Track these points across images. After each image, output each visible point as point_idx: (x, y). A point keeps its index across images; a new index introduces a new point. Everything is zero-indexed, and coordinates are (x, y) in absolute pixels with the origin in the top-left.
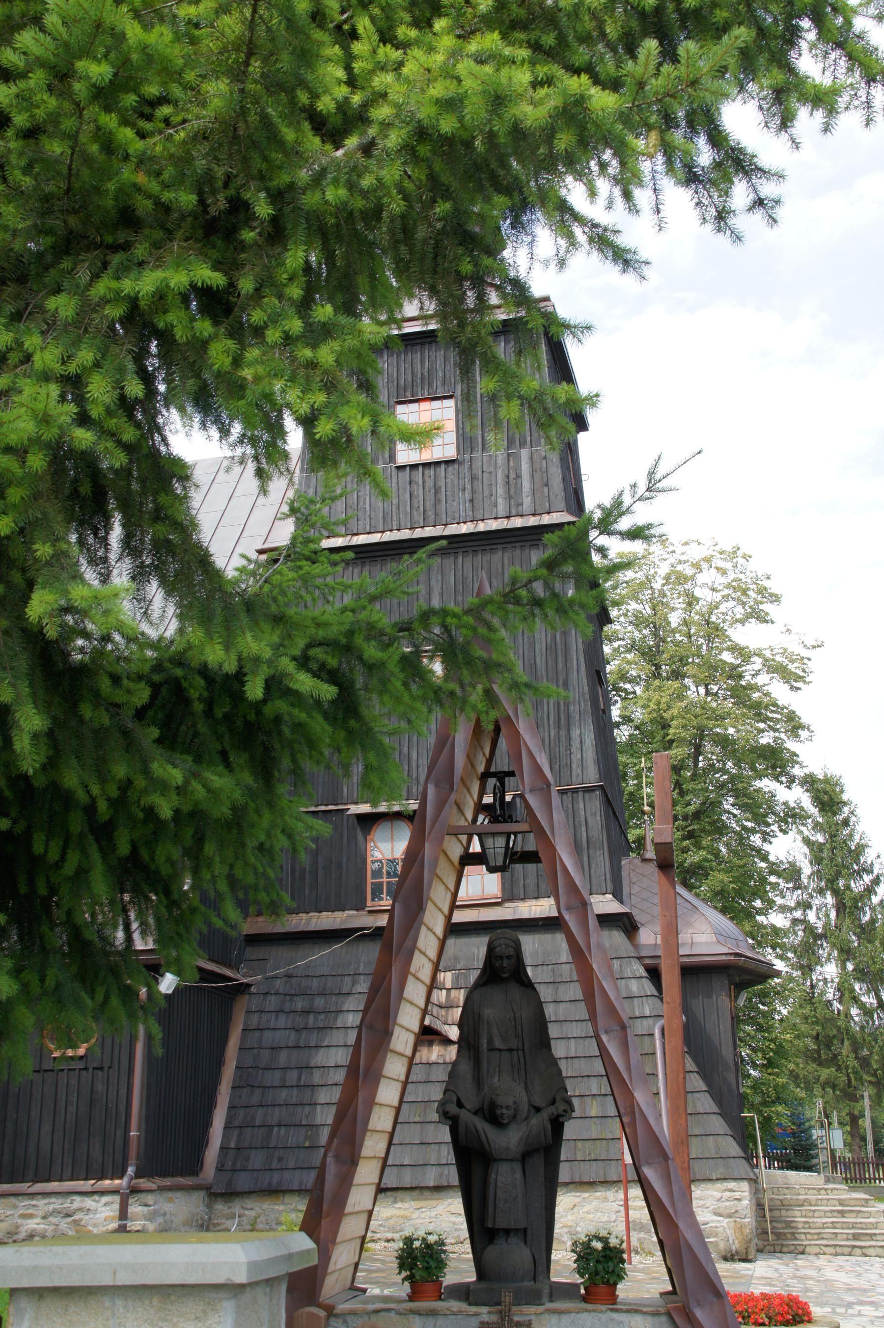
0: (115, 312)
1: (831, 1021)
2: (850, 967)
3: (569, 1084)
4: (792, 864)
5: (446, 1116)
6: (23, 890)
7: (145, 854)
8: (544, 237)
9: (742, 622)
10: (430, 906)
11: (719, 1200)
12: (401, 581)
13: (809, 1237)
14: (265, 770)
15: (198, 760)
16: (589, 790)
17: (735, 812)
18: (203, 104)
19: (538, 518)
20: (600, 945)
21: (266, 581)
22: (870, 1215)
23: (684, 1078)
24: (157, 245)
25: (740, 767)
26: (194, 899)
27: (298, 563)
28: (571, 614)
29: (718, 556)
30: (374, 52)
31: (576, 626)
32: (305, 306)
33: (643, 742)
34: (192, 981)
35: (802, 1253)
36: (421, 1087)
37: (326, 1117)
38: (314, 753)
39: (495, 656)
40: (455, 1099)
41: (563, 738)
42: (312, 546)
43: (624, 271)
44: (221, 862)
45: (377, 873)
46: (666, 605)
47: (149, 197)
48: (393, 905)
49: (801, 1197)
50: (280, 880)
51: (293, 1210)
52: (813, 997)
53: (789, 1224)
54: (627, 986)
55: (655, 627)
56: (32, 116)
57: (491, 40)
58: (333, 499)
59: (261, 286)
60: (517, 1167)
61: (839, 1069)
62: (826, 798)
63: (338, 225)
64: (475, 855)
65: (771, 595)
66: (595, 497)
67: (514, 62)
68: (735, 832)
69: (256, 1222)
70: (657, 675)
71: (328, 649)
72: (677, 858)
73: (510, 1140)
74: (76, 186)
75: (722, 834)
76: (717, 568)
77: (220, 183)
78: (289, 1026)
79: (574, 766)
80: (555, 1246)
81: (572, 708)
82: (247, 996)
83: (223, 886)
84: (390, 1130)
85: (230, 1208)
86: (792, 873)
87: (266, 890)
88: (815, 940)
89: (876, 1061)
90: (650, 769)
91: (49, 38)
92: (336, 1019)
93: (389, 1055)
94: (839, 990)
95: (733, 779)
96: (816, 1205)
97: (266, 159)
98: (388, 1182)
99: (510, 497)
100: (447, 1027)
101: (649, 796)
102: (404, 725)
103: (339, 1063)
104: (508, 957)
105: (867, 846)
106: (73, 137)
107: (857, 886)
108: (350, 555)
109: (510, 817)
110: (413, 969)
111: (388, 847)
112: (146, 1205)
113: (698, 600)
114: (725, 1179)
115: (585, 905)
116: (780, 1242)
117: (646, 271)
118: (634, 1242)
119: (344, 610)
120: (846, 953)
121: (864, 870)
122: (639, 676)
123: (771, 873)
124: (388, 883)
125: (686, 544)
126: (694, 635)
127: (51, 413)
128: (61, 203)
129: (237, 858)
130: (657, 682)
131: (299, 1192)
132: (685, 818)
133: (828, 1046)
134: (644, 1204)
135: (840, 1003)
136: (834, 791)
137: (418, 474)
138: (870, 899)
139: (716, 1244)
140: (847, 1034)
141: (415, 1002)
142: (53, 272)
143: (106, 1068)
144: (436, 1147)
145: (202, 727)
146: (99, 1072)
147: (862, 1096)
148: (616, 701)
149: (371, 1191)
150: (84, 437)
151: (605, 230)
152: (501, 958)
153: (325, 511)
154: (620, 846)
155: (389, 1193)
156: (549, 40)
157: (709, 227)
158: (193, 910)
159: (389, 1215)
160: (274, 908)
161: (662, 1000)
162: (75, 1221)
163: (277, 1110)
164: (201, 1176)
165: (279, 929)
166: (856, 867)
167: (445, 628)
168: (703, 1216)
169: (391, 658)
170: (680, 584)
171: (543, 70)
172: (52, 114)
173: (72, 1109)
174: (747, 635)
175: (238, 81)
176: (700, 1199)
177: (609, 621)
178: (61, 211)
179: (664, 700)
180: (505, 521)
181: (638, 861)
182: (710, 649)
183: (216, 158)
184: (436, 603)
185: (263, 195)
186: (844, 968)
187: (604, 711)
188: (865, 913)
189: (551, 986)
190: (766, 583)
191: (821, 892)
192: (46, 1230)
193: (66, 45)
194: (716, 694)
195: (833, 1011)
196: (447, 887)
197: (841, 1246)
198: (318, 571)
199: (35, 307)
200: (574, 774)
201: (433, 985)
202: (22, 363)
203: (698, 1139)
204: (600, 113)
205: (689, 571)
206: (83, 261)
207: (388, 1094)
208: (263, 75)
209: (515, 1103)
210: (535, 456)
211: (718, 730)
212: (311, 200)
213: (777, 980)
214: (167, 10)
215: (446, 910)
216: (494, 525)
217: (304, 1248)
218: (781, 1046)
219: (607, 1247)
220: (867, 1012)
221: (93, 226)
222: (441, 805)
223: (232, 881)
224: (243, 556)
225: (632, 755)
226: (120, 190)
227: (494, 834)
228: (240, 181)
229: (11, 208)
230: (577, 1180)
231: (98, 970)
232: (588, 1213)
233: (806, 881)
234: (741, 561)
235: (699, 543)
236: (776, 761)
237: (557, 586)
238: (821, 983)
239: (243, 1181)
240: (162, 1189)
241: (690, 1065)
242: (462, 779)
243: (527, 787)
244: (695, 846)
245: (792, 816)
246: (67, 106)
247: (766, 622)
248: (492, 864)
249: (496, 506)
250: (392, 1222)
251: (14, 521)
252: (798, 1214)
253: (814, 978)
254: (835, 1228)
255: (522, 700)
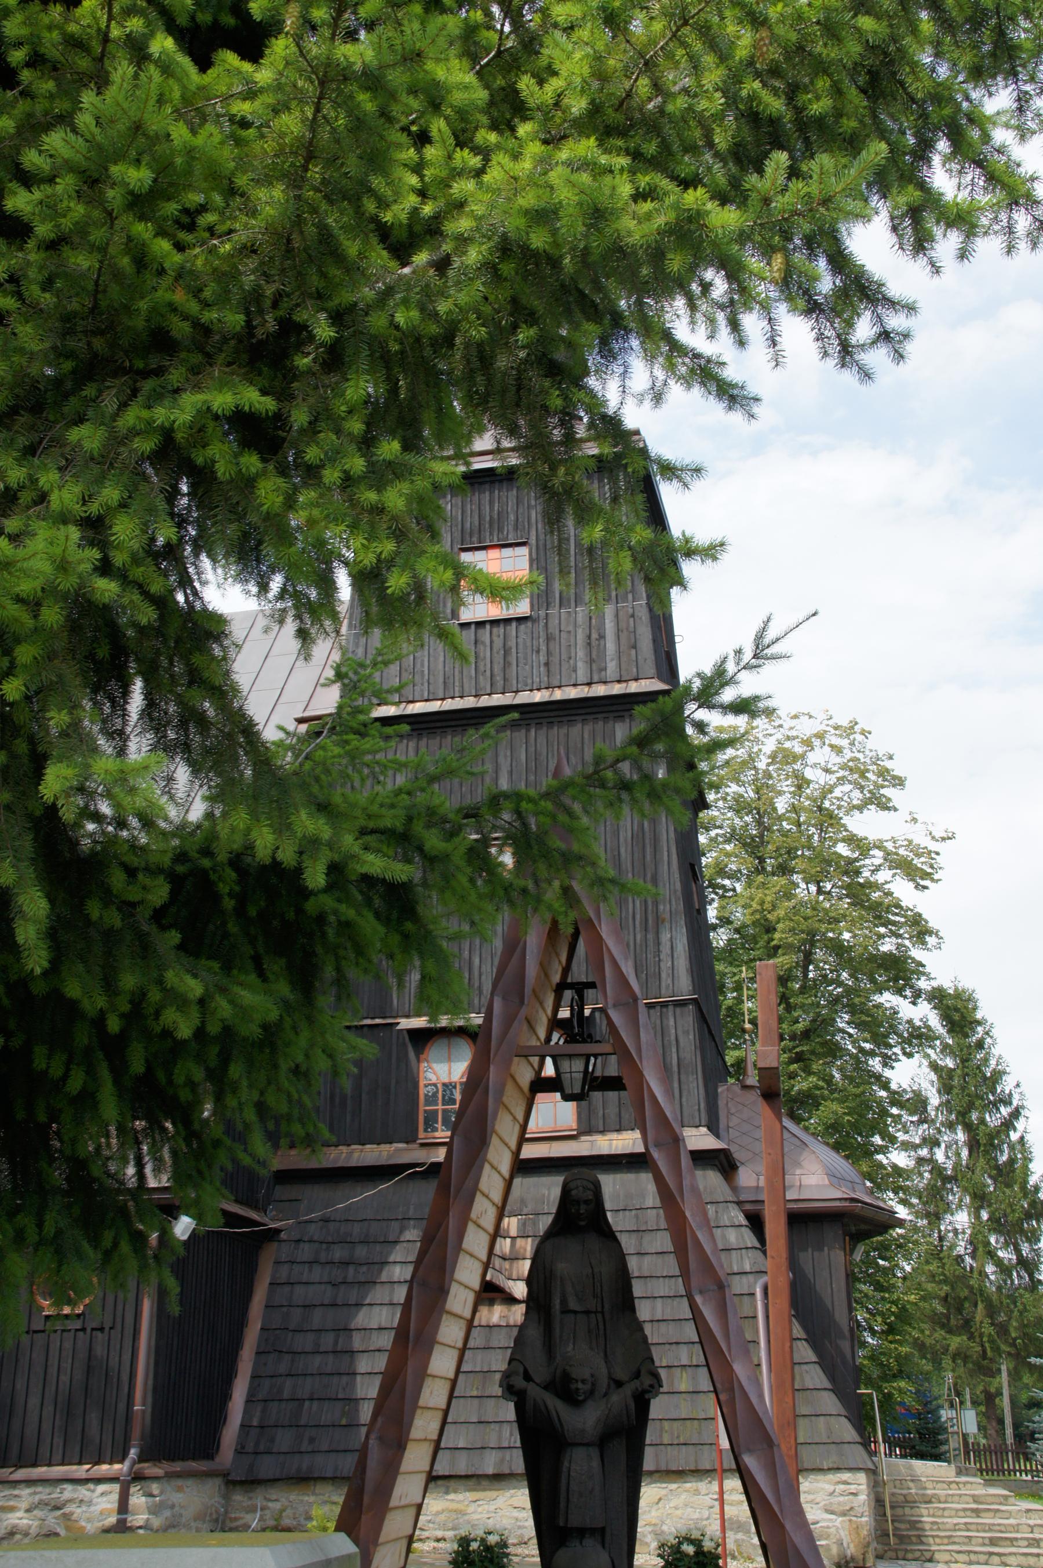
0: (146, 445)
1: (963, 1278)
2: (985, 1215)
3: (655, 1352)
4: (917, 1094)
5: (510, 1390)
6: (20, 1115)
7: (161, 1076)
8: (641, 371)
9: (860, 808)
10: (495, 1141)
11: (832, 1494)
12: (465, 760)
13: (938, 1540)
14: (305, 979)
15: (227, 967)
16: (681, 1004)
17: (851, 1031)
18: (253, 213)
19: (624, 685)
20: (695, 1189)
21: (307, 758)
22: (1009, 1515)
23: (791, 1347)
24: (195, 370)
25: (857, 979)
26: (217, 1131)
27: (345, 737)
28: (665, 799)
29: (833, 731)
30: (450, 157)
31: (669, 812)
32: (367, 443)
33: (744, 948)
34: (215, 1224)
35: (930, 1560)
36: (480, 1355)
37: (369, 1389)
38: (361, 960)
39: (576, 847)
40: (521, 1370)
41: (651, 943)
42: (361, 717)
43: (730, 408)
44: (250, 1086)
45: (431, 1099)
46: (771, 788)
47: (186, 318)
48: (452, 1138)
49: (929, 1492)
50: (317, 1110)
51: (324, 1505)
52: (941, 1251)
53: (914, 1525)
54: (724, 1237)
55: (758, 813)
56: (57, 226)
57: (586, 147)
58: (386, 663)
59: (316, 419)
60: (594, 1452)
61: (971, 1337)
62: (956, 1017)
63: (402, 352)
64: (549, 1079)
65: (894, 777)
66: (692, 662)
67: (611, 172)
68: (851, 1055)
69: (281, 1517)
70: (760, 870)
71: (383, 838)
72: (784, 1086)
73: (587, 1420)
74: (103, 304)
75: (835, 1057)
76: (831, 746)
77: (268, 303)
78: (325, 1279)
79: (664, 975)
80: (637, 1548)
81: (661, 907)
82: (275, 1244)
83: (250, 1115)
84: (444, 1407)
85: (250, 1498)
86: (917, 1104)
87: (301, 1120)
88: (944, 1184)
89: (1016, 1328)
90: (752, 980)
91: (81, 140)
92: (380, 1271)
93: (444, 1316)
94: (971, 1243)
95: (848, 991)
96: (946, 1502)
97: (323, 275)
98: (440, 1469)
99: (592, 661)
100: (511, 1283)
101: (750, 1011)
102: (466, 928)
103: (383, 1325)
104: (586, 1202)
105: (1005, 1073)
106: (102, 249)
107: (993, 1120)
108: (405, 728)
109: (590, 1036)
110: (473, 1215)
111: (445, 1070)
112: (151, 1495)
113: (808, 782)
114: (838, 1469)
115: (677, 1141)
116: (903, 1547)
117: (756, 409)
118: (731, 1545)
119: (398, 792)
120: (980, 1199)
121: (1001, 1101)
122: (740, 871)
123: (894, 1103)
124: (444, 1111)
125: (796, 717)
126: (804, 823)
127: (70, 559)
128: (85, 323)
129: (269, 1083)
130: (760, 878)
131: (334, 1479)
132: (793, 1038)
133: (959, 1310)
134: (743, 1498)
135: (973, 1258)
136: (966, 1008)
137: (485, 634)
138: (1008, 1136)
139: (827, 1548)
140: (981, 1295)
141: (476, 1253)
142: (73, 400)
143: (107, 1330)
144: (496, 1427)
145: (233, 927)
146: (99, 1334)
147: (999, 1371)
148: (713, 900)
149: (421, 1480)
150: (106, 588)
151: (709, 361)
152: (578, 1202)
153: (377, 675)
154: (716, 1070)
155: (440, 1482)
156: (651, 148)
157: (832, 362)
158: (217, 1144)
159: (440, 1508)
160: (310, 1141)
161: (764, 1253)
162: (64, 1514)
163: (309, 1379)
164: (217, 1459)
165: (314, 1164)
166: (991, 1098)
167: (518, 813)
168: (812, 1514)
169: (457, 849)
170: (788, 763)
171: (644, 180)
172: (77, 223)
173: (65, 1378)
174: (866, 824)
175: (295, 187)
176: (808, 1492)
177: (706, 806)
178: (85, 332)
179: (769, 899)
180: (586, 689)
181: (737, 1089)
182: (822, 840)
183: (265, 274)
184: (504, 785)
185: (323, 316)
186: (978, 1217)
187: (698, 911)
188: (1002, 1152)
189: (634, 1235)
190: (888, 764)
191: (951, 1126)
192: (30, 1527)
193: (100, 147)
194: (829, 893)
195: (964, 1268)
196: (515, 1118)
197: (975, 1553)
198: (368, 746)
199: (52, 440)
200: (663, 984)
201: (497, 1233)
202: (36, 503)
203: (806, 1420)
204: (720, 231)
205: (798, 749)
206: (109, 387)
207: (442, 1363)
208: (324, 181)
209: (592, 1376)
210: (621, 613)
211: (831, 935)
212: (378, 322)
213: (899, 1231)
214: (210, 109)
215: (513, 1145)
216: (573, 693)
217: (344, 1553)
218: (904, 1309)
219: (699, 1552)
220: (1004, 1269)
221: (117, 347)
222: (509, 1022)
223: (261, 1107)
224: (281, 728)
225: (731, 964)
226: (154, 310)
227: (570, 1056)
228: (295, 298)
229: (28, 329)
230: (663, 1468)
231: (104, 1215)
232: (676, 1508)
233: (933, 1113)
234: (859, 738)
235: (811, 717)
236: (899, 972)
237: (646, 762)
238: (951, 1235)
239: (267, 1467)
240: (170, 1476)
241: (798, 1331)
242: (534, 991)
243: (610, 1002)
244: (804, 1071)
245: (918, 1037)
246: (96, 214)
247: (888, 809)
248: (568, 1091)
249: (575, 671)
250: (442, 1517)
251: (25, 685)
252: (925, 1512)
253: (942, 1228)
254: (968, 1530)
255: (605, 899)
